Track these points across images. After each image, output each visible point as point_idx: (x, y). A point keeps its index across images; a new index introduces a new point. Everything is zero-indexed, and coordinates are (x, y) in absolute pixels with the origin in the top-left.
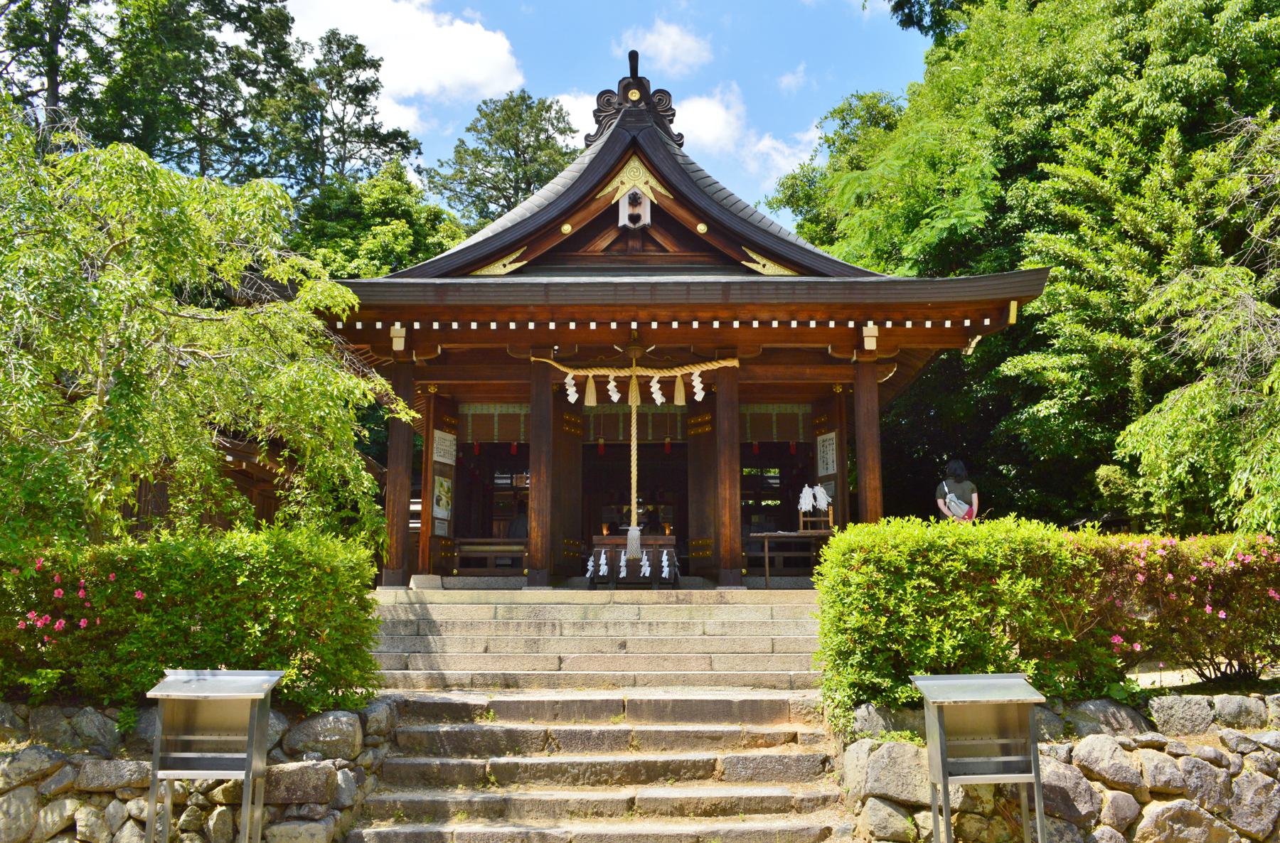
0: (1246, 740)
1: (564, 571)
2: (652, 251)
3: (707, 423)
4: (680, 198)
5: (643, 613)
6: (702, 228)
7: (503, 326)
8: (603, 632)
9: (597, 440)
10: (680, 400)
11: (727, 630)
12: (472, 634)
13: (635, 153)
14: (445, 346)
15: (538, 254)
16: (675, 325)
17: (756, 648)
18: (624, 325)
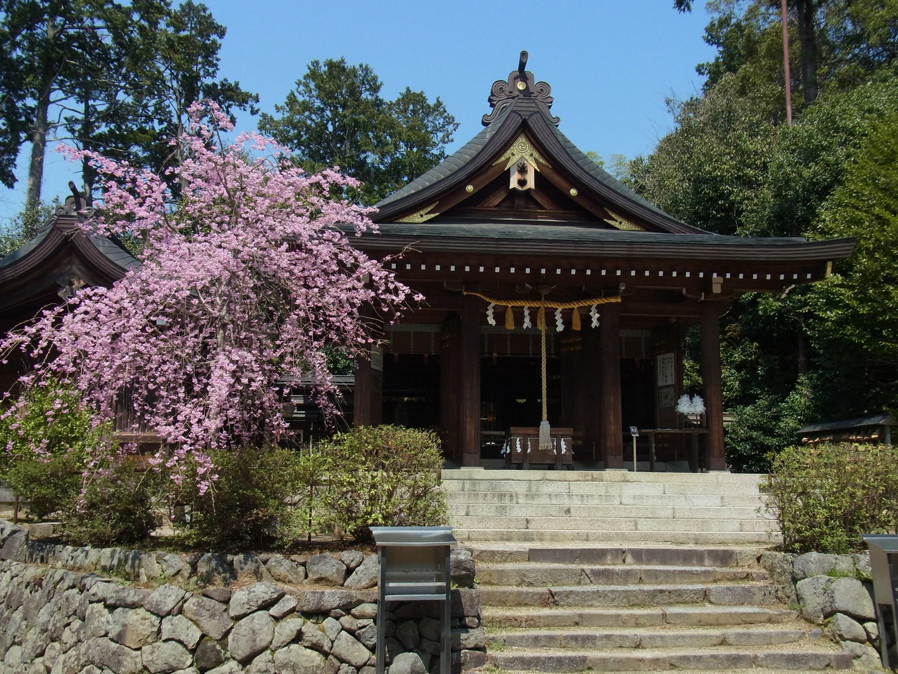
5: (572, 488)
6: (573, 192)
8: (547, 501)
10: (510, 325)
11: (637, 501)
13: (524, 132)
17: (662, 514)
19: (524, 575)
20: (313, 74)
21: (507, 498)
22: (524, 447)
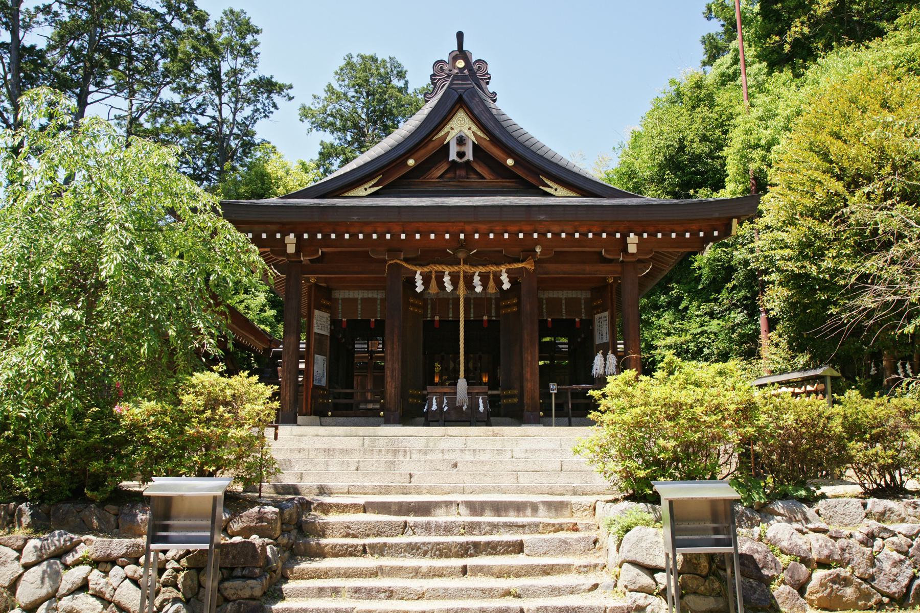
0: (885, 530)
1: (411, 413)
2: (474, 179)
3: (514, 305)
4: (494, 140)
5: (469, 443)
6: (510, 162)
7: (368, 236)
9: (433, 316)
11: (529, 455)
12: (346, 458)
14: (324, 250)
15: (391, 180)
16: (491, 236)
18: (455, 236)
19: (348, 527)
20: (350, 65)
21: (401, 454)
22: (440, 404)
